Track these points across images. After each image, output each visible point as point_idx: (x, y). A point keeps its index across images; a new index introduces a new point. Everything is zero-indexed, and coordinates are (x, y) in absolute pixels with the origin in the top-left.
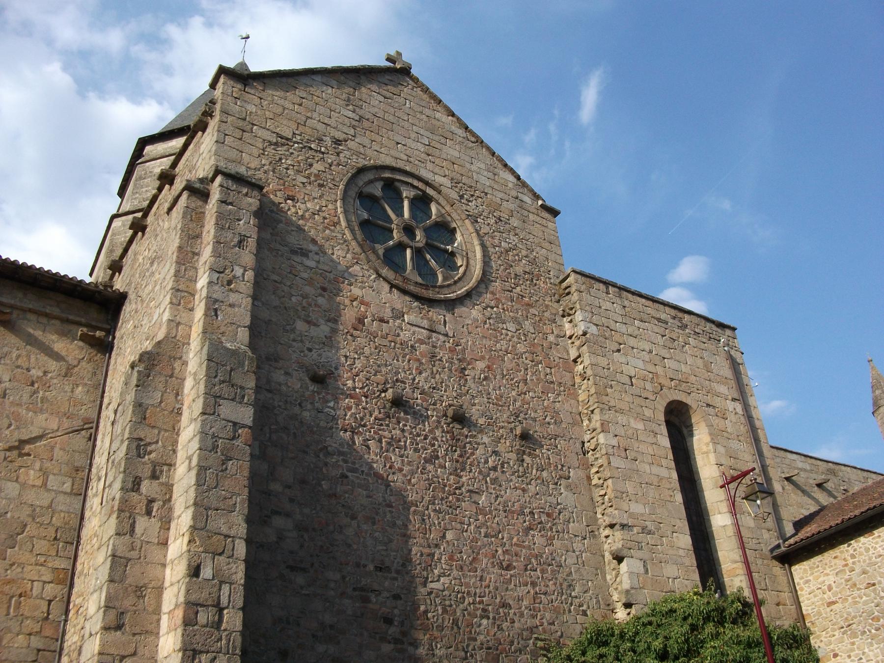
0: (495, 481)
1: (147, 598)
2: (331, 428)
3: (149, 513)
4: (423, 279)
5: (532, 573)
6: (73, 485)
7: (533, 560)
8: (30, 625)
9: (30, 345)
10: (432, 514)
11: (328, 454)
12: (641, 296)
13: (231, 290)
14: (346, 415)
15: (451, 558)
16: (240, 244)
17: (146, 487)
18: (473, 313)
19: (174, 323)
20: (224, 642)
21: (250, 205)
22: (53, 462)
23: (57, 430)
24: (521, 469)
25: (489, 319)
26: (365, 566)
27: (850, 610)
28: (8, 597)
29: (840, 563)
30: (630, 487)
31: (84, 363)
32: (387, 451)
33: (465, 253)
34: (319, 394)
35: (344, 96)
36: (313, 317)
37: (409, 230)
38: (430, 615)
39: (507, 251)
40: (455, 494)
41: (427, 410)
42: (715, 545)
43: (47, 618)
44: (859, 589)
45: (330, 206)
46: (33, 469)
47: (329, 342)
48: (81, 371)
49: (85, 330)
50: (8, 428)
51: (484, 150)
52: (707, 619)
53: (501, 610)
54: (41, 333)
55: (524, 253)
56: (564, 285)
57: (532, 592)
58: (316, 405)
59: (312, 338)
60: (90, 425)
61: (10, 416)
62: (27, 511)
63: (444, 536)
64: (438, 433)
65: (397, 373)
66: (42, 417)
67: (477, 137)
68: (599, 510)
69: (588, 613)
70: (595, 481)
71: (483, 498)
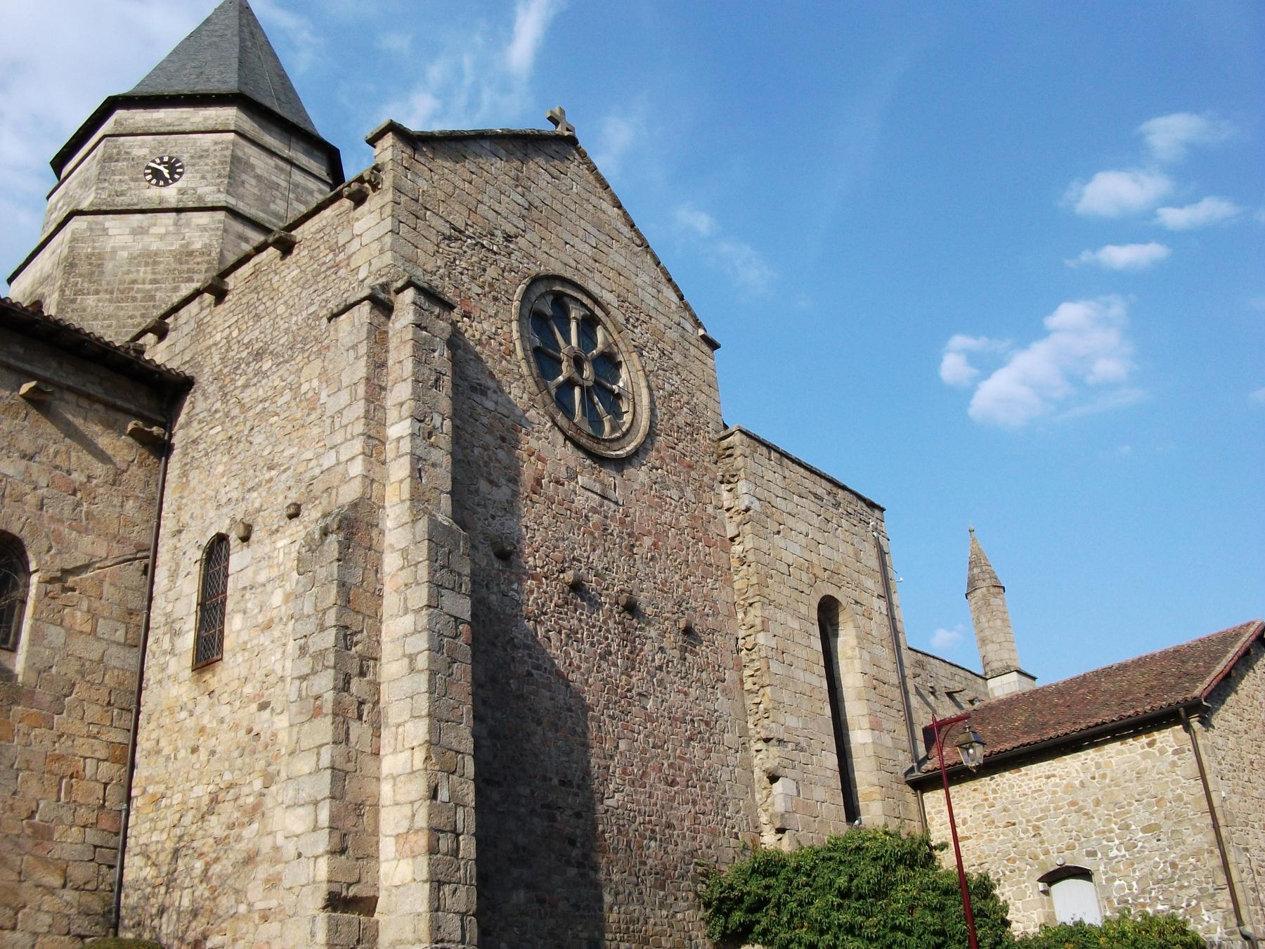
0: (661, 682)
1: (365, 817)
2: (516, 616)
3: (360, 717)
4: (593, 430)
5: (693, 790)
6: (127, 633)
7: (694, 775)
8: (85, 815)
9: (70, 437)
10: (607, 720)
11: (515, 647)
12: (800, 464)
13: (432, 445)
14: (528, 600)
15: (624, 772)
16: (436, 384)
17: (355, 684)
18: (640, 475)
19: (368, 480)
20: (462, 871)
21: (443, 330)
22: (103, 601)
23: (106, 558)
24: (683, 668)
25: (655, 483)
26: (550, 779)
27: (985, 848)
28: (58, 777)
29: (979, 797)
30: (785, 696)
31: (134, 468)
32: (567, 645)
33: (631, 396)
34: (504, 573)
35: (513, 173)
36: (494, 476)
37: (578, 363)
38: (607, 835)
39: (671, 395)
40: (626, 697)
41: (601, 595)
42: (852, 764)
43: (103, 806)
44: (997, 827)
45: (505, 328)
46: (80, 610)
47: (510, 508)
48: (132, 478)
49: (140, 423)
50: (48, 551)
51: (649, 257)
52: (900, 861)
53: (667, 831)
54: (82, 422)
55: (685, 398)
56: (725, 443)
57: (693, 811)
58: (502, 586)
59: (495, 502)
60: (145, 554)
61: (50, 535)
62: (74, 666)
63: (617, 747)
64: (611, 623)
65: (573, 549)
66: (88, 539)
67: (643, 240)
68: (751, 720)
69: (740, 836)
70: (748, 685)
71: (651, 702)
